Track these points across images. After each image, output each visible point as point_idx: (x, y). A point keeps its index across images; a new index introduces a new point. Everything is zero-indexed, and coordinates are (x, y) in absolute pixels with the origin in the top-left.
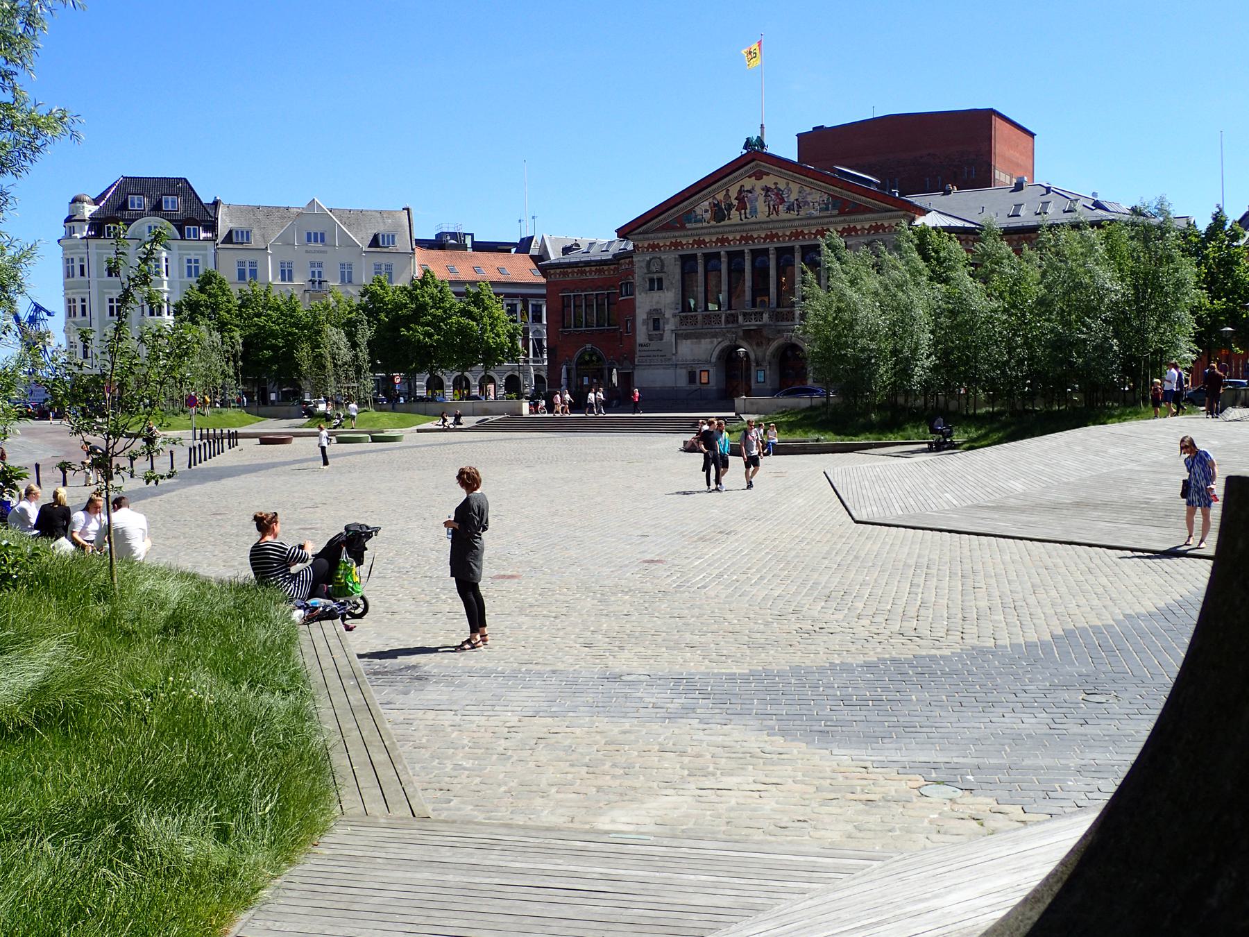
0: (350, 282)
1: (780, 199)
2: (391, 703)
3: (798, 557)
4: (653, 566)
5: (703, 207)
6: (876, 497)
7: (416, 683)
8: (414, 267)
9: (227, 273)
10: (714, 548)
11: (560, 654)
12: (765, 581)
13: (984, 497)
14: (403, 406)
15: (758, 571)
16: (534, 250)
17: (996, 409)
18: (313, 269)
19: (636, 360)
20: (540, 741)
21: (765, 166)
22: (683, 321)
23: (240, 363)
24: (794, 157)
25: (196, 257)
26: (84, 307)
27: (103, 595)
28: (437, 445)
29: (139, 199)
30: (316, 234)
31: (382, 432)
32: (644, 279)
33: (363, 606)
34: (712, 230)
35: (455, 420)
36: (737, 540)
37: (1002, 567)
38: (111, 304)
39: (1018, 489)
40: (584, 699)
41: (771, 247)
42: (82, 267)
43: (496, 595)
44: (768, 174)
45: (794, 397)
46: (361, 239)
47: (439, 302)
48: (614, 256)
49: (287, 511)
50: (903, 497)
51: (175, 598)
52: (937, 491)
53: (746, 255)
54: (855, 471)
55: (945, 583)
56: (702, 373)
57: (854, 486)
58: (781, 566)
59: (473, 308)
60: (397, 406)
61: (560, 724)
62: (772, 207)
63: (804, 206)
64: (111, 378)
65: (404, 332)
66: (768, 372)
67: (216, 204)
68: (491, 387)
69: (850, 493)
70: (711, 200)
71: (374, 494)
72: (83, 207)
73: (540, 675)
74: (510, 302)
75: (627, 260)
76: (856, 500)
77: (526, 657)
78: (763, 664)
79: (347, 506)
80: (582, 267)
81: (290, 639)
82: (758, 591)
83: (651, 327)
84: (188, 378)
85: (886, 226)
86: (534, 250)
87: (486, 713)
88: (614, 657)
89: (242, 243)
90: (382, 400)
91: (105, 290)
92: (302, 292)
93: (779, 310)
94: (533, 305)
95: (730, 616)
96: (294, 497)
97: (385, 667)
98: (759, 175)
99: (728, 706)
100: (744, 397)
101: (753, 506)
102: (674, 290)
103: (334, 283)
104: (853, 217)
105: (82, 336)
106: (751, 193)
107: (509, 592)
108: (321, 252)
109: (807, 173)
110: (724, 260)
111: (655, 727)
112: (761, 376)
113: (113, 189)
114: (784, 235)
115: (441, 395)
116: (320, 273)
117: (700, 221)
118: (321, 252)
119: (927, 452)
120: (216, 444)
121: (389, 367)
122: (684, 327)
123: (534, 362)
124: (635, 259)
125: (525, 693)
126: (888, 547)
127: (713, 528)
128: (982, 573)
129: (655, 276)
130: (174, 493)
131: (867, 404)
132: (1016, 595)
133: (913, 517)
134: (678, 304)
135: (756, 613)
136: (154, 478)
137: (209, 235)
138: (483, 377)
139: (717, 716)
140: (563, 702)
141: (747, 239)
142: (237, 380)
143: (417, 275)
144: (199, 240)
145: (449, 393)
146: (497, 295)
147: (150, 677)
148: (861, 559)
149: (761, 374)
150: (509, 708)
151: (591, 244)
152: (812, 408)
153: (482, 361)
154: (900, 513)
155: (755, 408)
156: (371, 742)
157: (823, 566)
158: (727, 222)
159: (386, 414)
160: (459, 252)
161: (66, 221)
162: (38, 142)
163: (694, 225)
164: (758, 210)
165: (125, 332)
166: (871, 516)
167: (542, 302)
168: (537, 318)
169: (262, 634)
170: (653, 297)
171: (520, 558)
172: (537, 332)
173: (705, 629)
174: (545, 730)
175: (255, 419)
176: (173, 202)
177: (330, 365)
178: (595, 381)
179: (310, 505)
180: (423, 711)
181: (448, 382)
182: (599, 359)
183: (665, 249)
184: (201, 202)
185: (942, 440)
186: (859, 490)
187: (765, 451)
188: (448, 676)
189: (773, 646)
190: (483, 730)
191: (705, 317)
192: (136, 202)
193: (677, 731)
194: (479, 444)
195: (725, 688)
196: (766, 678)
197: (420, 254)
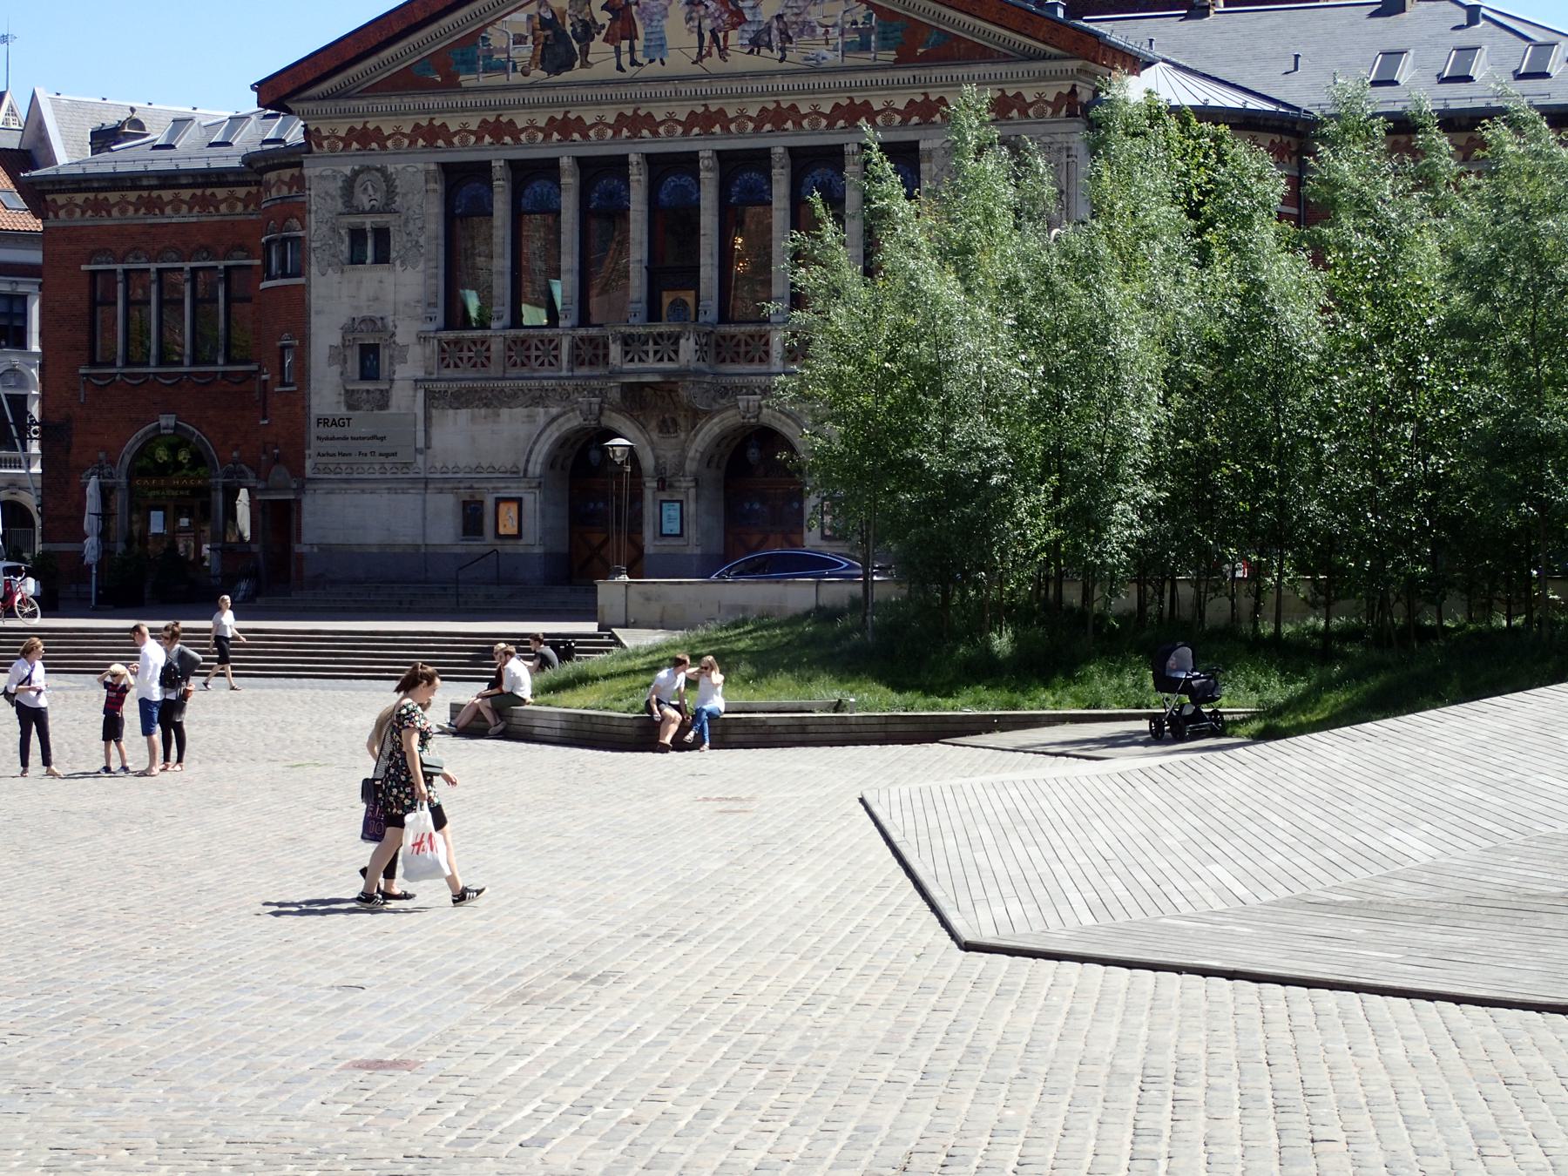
1: (732, 13)
3: (806, 1049)
4: (383, 1080)
6: (1015, 871)
10: (559, 1022)
12: (717, 1123)
13: (1322, 876)
15: (695, 1092)
17: (1335, 621)
19: (308, 464)
22: (448, 354)
32: (334, 230)
34: (535, 95)
36: (625, 1001)
37: (1385, 1078)
39: (1412, 853)
45: (770, 580)
48: (249, 160)
50: (1091, 873)
52: (1186, 857)
53: (633, 170)
54: (949, 796)
55: (1231, 1128)
56: (503, 507)
57: (950, 842)
58: (760, 1076)
62: (707, 35)
66: (691, 508)
69: (941, 861)
70: (533, 9)
75: (286, 174)
76: (960, 882)
80: (150, 188)
85: (1029, 99)
100: (625, 578)
101: (666, 898)
102: (421, 266)
104: (937, 72)
110: (569, 180)
117: (502, 68)
119: (1146, 743)
122: (447, 373)
124: (306, 172)
126: (1060, 1021)
127: (552, 964)
128: (1332, 1096)
129: (368, 222)
131: (981, 605)
132: (1430, 1160)
133: (1124, 933)
134: (435, 305)
148: (986, 1058)
151: (180, 123)
152: (824, 614)
154: (1088, 920)
155: (655, 610)
157: (882, 1077)
158: (577, 73)
163: (484, 80)
164: (669, 45)
166: (1022, 929)
167: (26, 287)
170: (360, 282)
182: (198, 459)
183: (398, 145)
185: (1188, 711)
186: (965, 851)
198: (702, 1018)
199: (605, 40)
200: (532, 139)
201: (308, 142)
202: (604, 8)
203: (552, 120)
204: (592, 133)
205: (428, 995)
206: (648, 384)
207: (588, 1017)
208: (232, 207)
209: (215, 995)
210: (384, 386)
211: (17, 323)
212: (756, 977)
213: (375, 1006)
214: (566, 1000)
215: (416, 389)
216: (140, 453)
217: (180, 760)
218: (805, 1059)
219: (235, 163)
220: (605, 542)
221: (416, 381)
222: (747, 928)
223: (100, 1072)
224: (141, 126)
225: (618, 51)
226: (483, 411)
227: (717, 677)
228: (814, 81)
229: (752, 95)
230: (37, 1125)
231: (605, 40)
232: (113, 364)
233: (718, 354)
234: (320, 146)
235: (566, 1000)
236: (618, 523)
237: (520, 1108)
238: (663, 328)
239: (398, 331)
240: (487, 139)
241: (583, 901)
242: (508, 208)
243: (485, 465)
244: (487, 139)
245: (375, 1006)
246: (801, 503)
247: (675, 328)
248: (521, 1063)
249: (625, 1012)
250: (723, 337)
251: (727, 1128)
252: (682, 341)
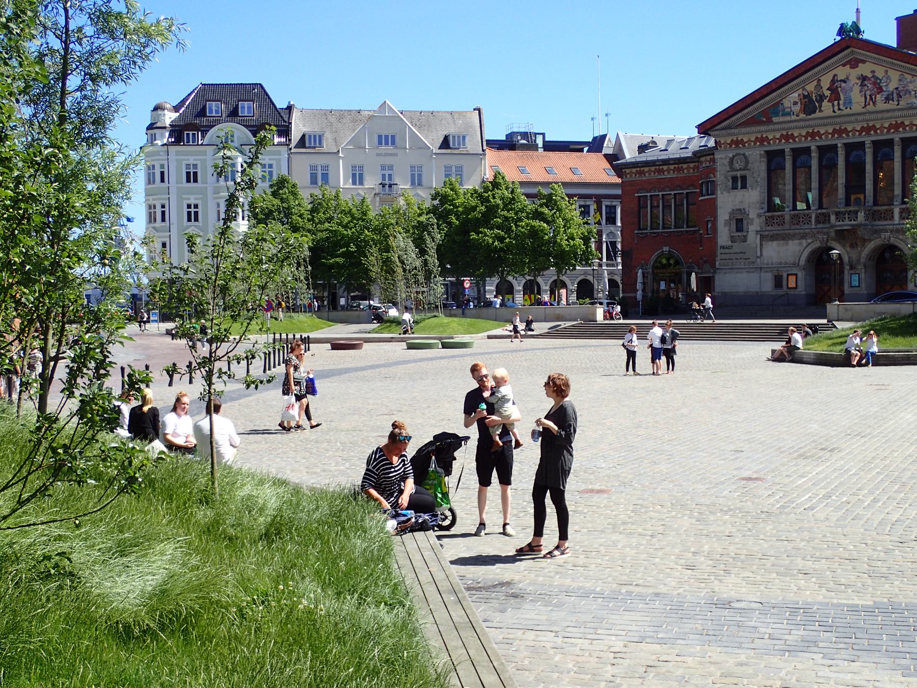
0: (420, 184)
1: (878, 88)
2: (488, 621)
4: (752, 485)
5: (792, 99)
7: (513, 601)
8: (485, 169)
9: (300, 177)
10: (817, 466)
11: (661, 575)
12: (880, 504)
14: (474, 311)
15: (871, 492)
16: (608, 148)
18: (384, 172)
19: (717, 263)
20: (649, 669)
21: (860, 53)
22: (769, 221)
23: (310, 268)
24: (892, 42)
25: (271, 162)
26: (163, 213)
27: (206, 500)
28: (509, 351)
29: (217, 106)
30: (387, 137)
31: (452, 338)
33: (450, 518)
34: (802, 124)
35: (526, 326)
38: (189, 210)
40: (691, 626)
41: (868, 140)
42: (162, 173)
43: (586, 511)
44: (864, 62)
46: (432, 141)
47: (509, 203)
48: (695, 153)
49: (364, 418)
51: (273, 504)
56: (790, 277)
58: (896, 487)
59: (545, 210)
60: (467, 311)
61: (669, 652)
63: (906, 94)
64: (215, 282)
65: (473, 236)
66: (863, 276)
67: (290, 108)
68: (563, 292)
70: (800, 91)
71: (448, 402)
72: (164, 115)
73: (642, 597)
74: (582, 203)
75: (708, 158)
77: (625, 577)
78: (889, 596)
79: (423, 414)
81: (386, 550)
82: (872, 514)
83: (734, 226)
84: (289, 283)
85: (822, 132)
86: (608, 148)
87: (589, 636)
88: (720, 581)
89: (314, 148)
90: (452, 305)
91: (183, 196)
92: (372, 196)
93: (876, 208)
94: (606, 206)
95: (845, 542)
96: (369, 403)
97: (479, 583)
98: (854, 63)
99: (853, 640)
100: (837, 303)
101: (856, 421)
102: (758, 189)
103: (403, 185)
105: (189, 241)
106: (845, 82)
107: (599, 507)
108: (391, 155)
109: (908, 59)
110: (815, 155)
111: (775, 660)
112: (854, 280)
113: (193, 96)
114: (882, 127)
115: (511, 300)
116: (390, 175)
117: (789, 114)
118: (391, 155)
120: (281, 352)
121: (459, 271)
122: (769, 228)
123: (608, 265)
124: (716, 157)
125: (628, 616)
129: (739, 174)
130: (251, 398)
134: (764, 203)
135: (873, 539)
136: (253, 383)
137: (283, 140)
138: (555, 281)
139: (843, 652)
140: (670, 628)
141: (840, 132)
142: (308, 285)
143: (487, 176)
144: (274, 145)
145: (519, 298)
146: (570, 196)
147: (264, 584)
149: (855, 278)
150: (612, 632)
151: (670, 141)
153: (556, 265)
155: (849, 314)
156: (479, 662)
158: (818, 114)
159: (456, 319)
160: (530, 153)
161: (148, 129)
162: (148, 50)
163: (782, 119)
165: (230, 237)
168: (611, 220)
169: (359, 544)
171: (608, 472)
172: (611, 234)
173: (818, 554)
174: (654, 657)
175: (325, 324)
176: (249, 108)
177: (399, 270)
178: (672, 285)
179: (386, 412)
180: (522, 631)
181: (518, 287)
182: (677, 263)
183: (749, 145)
184: (275, 107)
187: (864, 361)
188: (544, 594)
189: (897, 576)
190: (587, 654)
191: (793, 217)
192: (214, 109)
193: (799, 666)
194: (553, 351)
195: (848, 620)
196: (893, 611)
197: (491, 155)
198: (872, 465)
199: (828, 101)
200: (800, 140)
201: (716, 146)
202: (828, 89)
203: (808, 132)
204: (823, 137)
205: (767, 455)
206: (845, 230)
207: (828, 464)
208: (688, 171)
209: (689, 453)
210: (745, 234)
211: (613, 216)
212: (893, 451)
213: (748, 458)
214: (820, 457)
215: (757, 234)
216: (655, 262)
217: (673, 370)
218: (913, 481)
219: (690, 155)
220: (829, 290)
221: (757, 231)
222: (889, 432)
223: (649, 478)
224: (656, 143)
225: (833, 105)
226: (782, 242)
227: (875, 339)
228: (911, 112)
229: (886, 119)
230: (628, 496)
231: (828, 101)
232: (647, 229)
233: (873, 218)
234: (721, 147)
235: (820, 457)
236: (835, 282)
237: (804, 496)
238: (851, 208)
239: (750, 213)
240: (783, 141)
241: (825, 422)
242: (791, 166)
243: (783, 262)
244: (783, 141)
245: (748, 458)
246: (907, 273)
247: (856, 208)
248: (804, 480)
249: (842, 462)
250: (875, 211)
251: (884, 506)
252: (859, 213)
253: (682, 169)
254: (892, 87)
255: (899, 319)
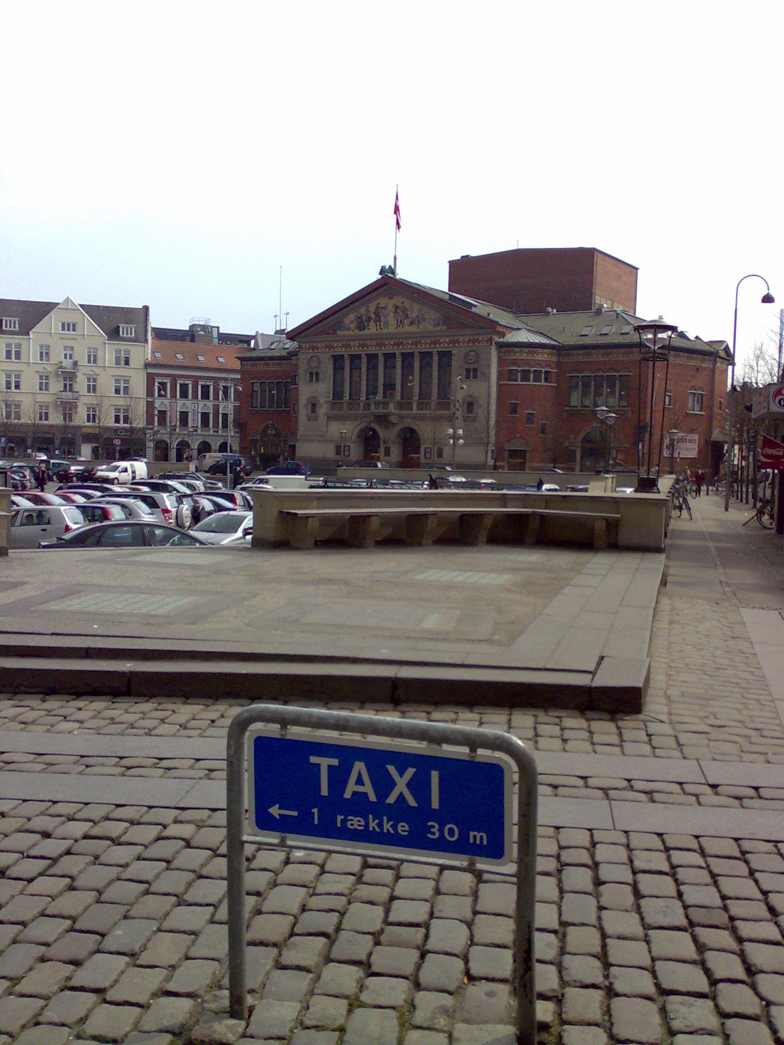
5: (350, 319)
22: (333, 405)
30: (69, 324)
44: (397, 295)
62: (399, 321)
85: (442, 341)
117: (347, 329)
129: (471, 367)
232: (257, 407)
253: (282, 364)
254: (415, 314)
255: (72, 458)
